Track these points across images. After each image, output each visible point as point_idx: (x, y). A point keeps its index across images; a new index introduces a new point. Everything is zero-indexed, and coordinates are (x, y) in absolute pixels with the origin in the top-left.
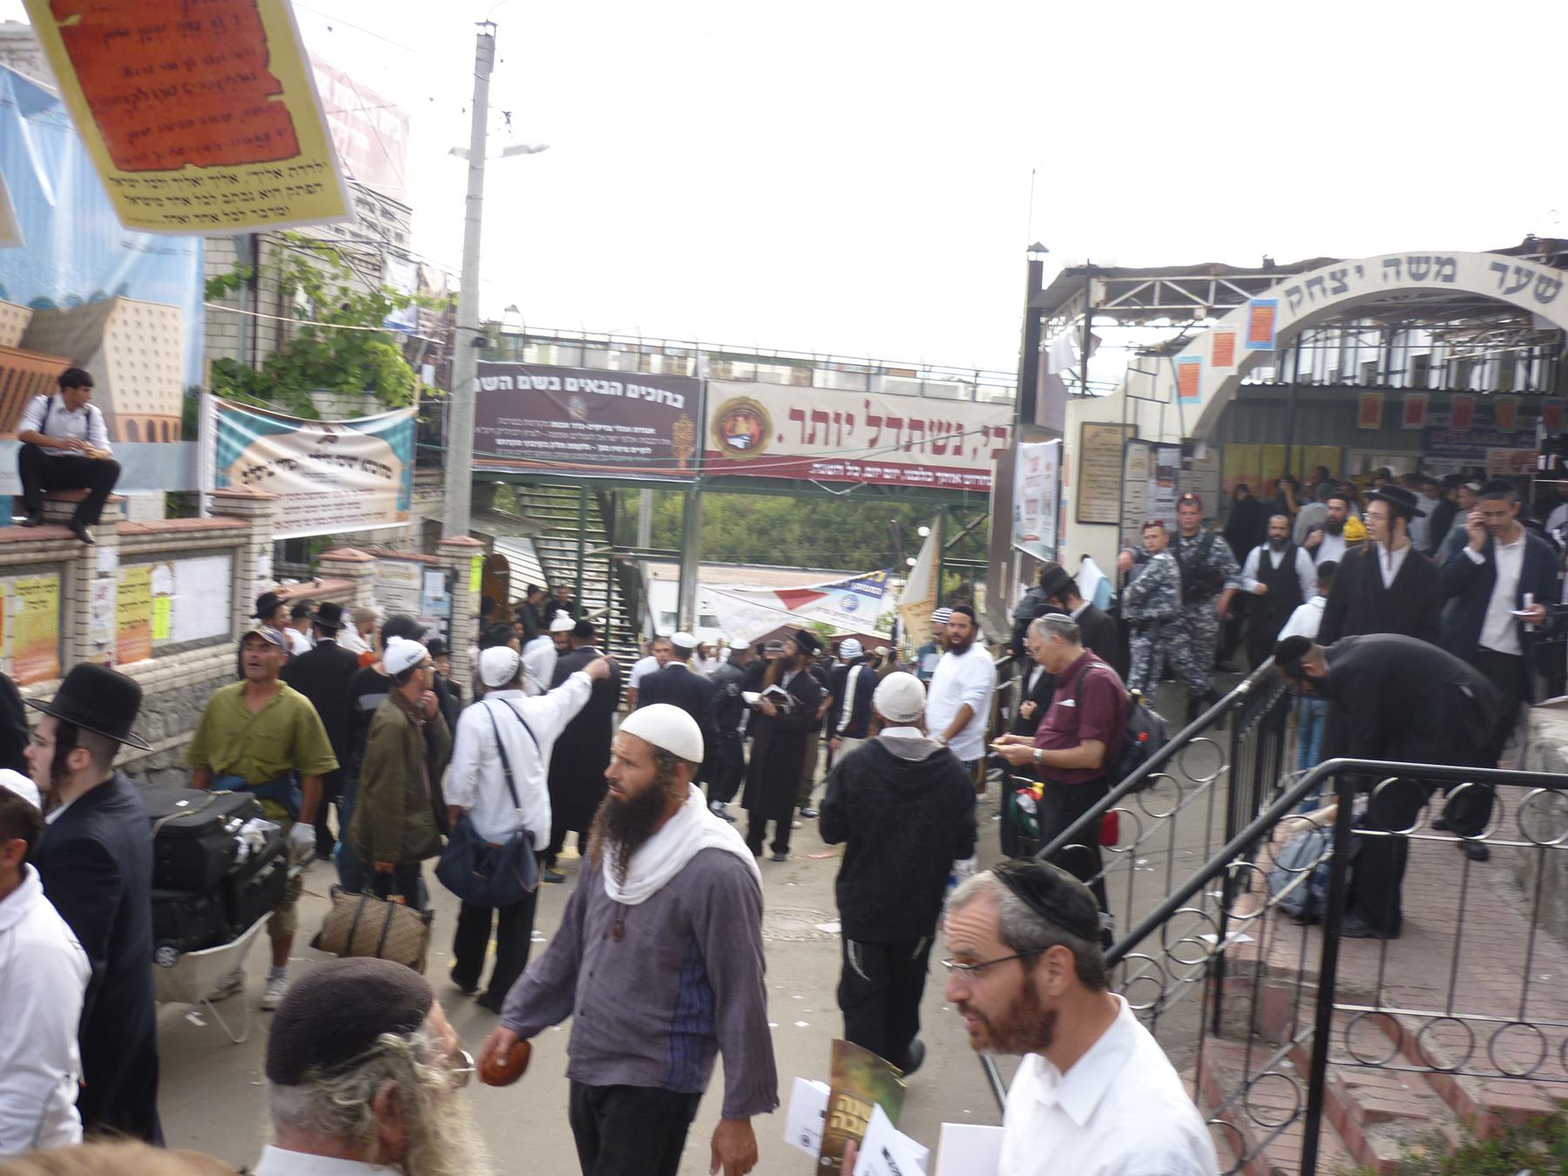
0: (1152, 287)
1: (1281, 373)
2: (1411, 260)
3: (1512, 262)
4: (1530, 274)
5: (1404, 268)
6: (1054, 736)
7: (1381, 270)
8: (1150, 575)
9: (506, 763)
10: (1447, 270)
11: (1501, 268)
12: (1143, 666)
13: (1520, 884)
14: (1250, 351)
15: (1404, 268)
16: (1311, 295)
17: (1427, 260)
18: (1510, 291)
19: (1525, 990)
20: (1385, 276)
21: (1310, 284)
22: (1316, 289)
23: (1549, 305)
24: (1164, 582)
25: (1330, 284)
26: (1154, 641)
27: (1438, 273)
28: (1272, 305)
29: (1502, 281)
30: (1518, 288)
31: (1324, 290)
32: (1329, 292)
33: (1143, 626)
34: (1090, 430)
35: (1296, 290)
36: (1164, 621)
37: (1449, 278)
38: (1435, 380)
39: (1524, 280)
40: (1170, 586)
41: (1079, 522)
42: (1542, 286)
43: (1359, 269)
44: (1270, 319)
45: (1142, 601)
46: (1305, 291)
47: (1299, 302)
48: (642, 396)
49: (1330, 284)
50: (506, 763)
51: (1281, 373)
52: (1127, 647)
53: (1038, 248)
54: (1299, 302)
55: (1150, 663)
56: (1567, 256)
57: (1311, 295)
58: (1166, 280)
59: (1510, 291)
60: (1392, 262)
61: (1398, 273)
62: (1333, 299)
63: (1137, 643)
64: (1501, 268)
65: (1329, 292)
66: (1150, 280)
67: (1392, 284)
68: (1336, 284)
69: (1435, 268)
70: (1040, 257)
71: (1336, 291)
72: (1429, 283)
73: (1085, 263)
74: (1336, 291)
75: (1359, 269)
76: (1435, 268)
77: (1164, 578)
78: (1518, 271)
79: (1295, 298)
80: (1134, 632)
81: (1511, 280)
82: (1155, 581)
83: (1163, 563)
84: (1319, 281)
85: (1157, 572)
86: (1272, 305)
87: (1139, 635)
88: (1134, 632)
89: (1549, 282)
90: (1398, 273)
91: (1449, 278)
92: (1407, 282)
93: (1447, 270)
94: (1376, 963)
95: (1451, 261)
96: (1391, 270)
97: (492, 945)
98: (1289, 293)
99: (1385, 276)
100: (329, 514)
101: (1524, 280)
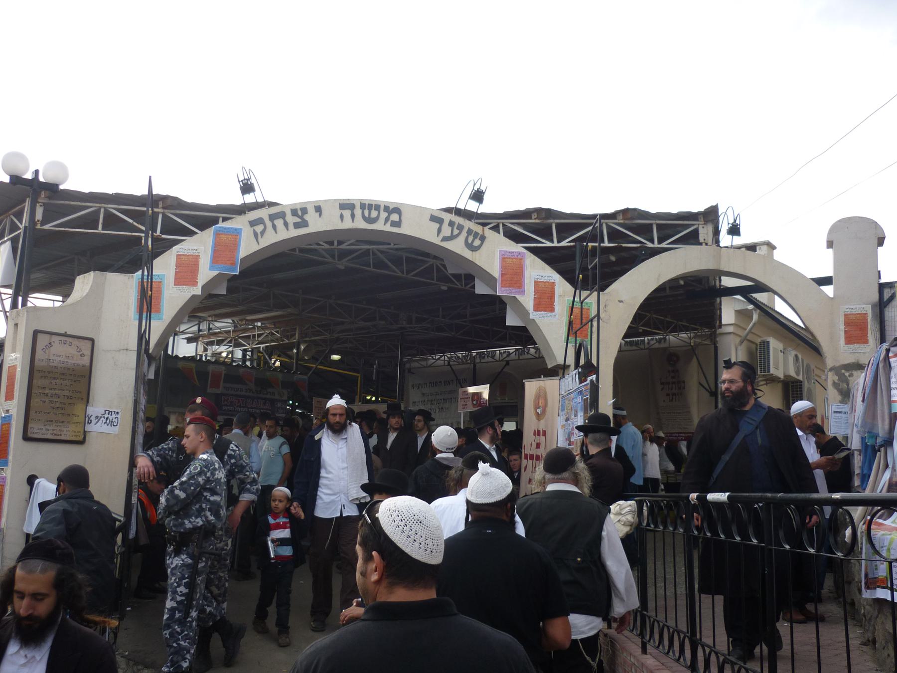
0: (97, 212)
2: (363, 206)
3: (447, 217)
4: (460, 228)
5: (358, 212)
7: (338, 212)
8: (192, 477)
10: (395, 217)
11: (440, 221)
12: (182, 589)
14: (215, 273)
15: (358, 212)
16: (274, 227)
17: (377, 207)
18: (445, 239)
20: (342, 217)
22: (279, 223)
24: (209, 486)
26: (196, 559)
27: (387, 219)
28: (237, 232)
29: (439, 231)
30: (452, 238)
31: (286, 224)
32: (291, 226)
33: (182, 542)
35: (260, 221)
36: (207, 531)
37: (397, 224)
40: (214, 492)
41: (26, 438)
42: (470, 239)
43: (318, 209)
44: (235, 246)
45: (181, 509)
47: (263, 233)
52: (163, 567)
54: (263, 233)
55: (192, 586)
57: (274, 227)
58: (112, 208)
59: (445, 239)
60: (347, 206)
61: (353, 216)
62: (294, 233)
63: (175, 562)
64: (440, 221)
65: (291, 226)
66: (93, 207)
67: (348, 224)
69: (384, 215)
72: (379, 226)
74: (297, 226)
75: (318, 209)
76: (384, 215)
77: (208, 481)
78: (451, 224)
79: (259, 228)
80: (170, 549)
81: (446, 231)
82: (198, 484)
83: (207, 464)
85: (200, 474)
86: (237, 232)
87: (177, 553)
88: (170, 549)
89: (476, 235)
90: (353, 216)
91: (394, 224)
92: (361, 224)
93: (395, 217)
95: (397, 210)
96: (347, 213)
97: (131, 221)
98: (253, 223)
99: (342, 217)
101: (456, 232)
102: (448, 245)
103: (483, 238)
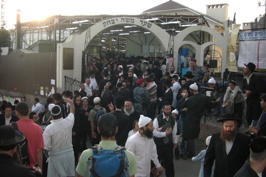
1: (258, 24)
15: (125, 20)
16: (108, 24)
18: (143, 25)
19: (258, 61)
21: (107, 22)
23: (150, 28)
25: (111, 22)
27: (131, 21)
29: (142, 24)
30: (145, 25)
31: (110, 23)
32: (111, 24)
34: (65, 50)
35: (105, 23)
38: (92, 48)
39: (145, 24)
46: (107, 23)
47: (105, 25)
49: (111, 22)
51: (258, 24)
53: (19, 11)
54: (105, 25)
57: (108, 24)
58: (187, 23)
59: (143, 25)
61: (124, 21)
62: (112, 25)
65: (111, 24)
66: (190, 23)
68: (113, 22)
69: (130, 20)
70: (19, 13)
71: (112, 23)
73: (59, 15)
74: (112, 23)
76: (130, 20)
79: (105, 24)
81: (143, 24)
84: (109, 21)
90: (124, 21)
93: (133, 21)
94: (250, 29)
96: (123, 20)
99: (122, 21)
103: (151, 25)
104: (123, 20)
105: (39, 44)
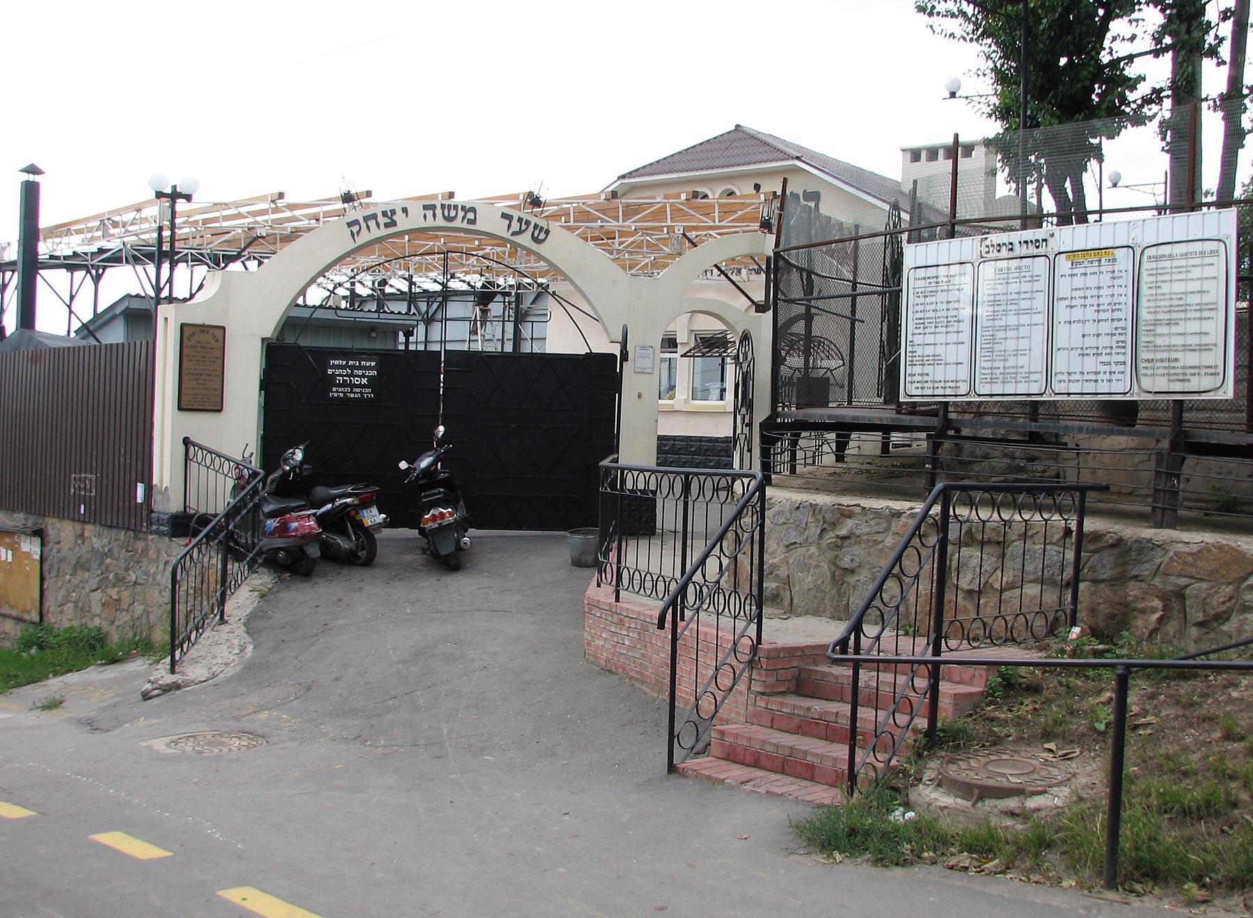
4: (528, 223)
5: (439, 212)
6: (861, 479)
9: (328, 268)
10: (470, 216)
13: (1100, 873)
15: (439, 212)
16: (368, 227)
18: (514, 234)
20: (425, 216)
29: (509, 226)
30: (520, 232)
37: (473, 222)
43: (405, 210)
48: (1213, 52)
49: (382, 220)
50: (328, 268)
54: (358, 233)
56: (39, 653)
57: (368, 227)
59: (514, 234)
71: (386, 225)
74: (386, 225)
79: (355, 229)
81: (515, 226)
93: (470, 216)
95: (473, 210)
96: (429, 213)
99: (425, 216)
100: (1176, 263)
102: (517, 239)
103: (547, 232)
104: (429, 213)
105: (122, 313)
